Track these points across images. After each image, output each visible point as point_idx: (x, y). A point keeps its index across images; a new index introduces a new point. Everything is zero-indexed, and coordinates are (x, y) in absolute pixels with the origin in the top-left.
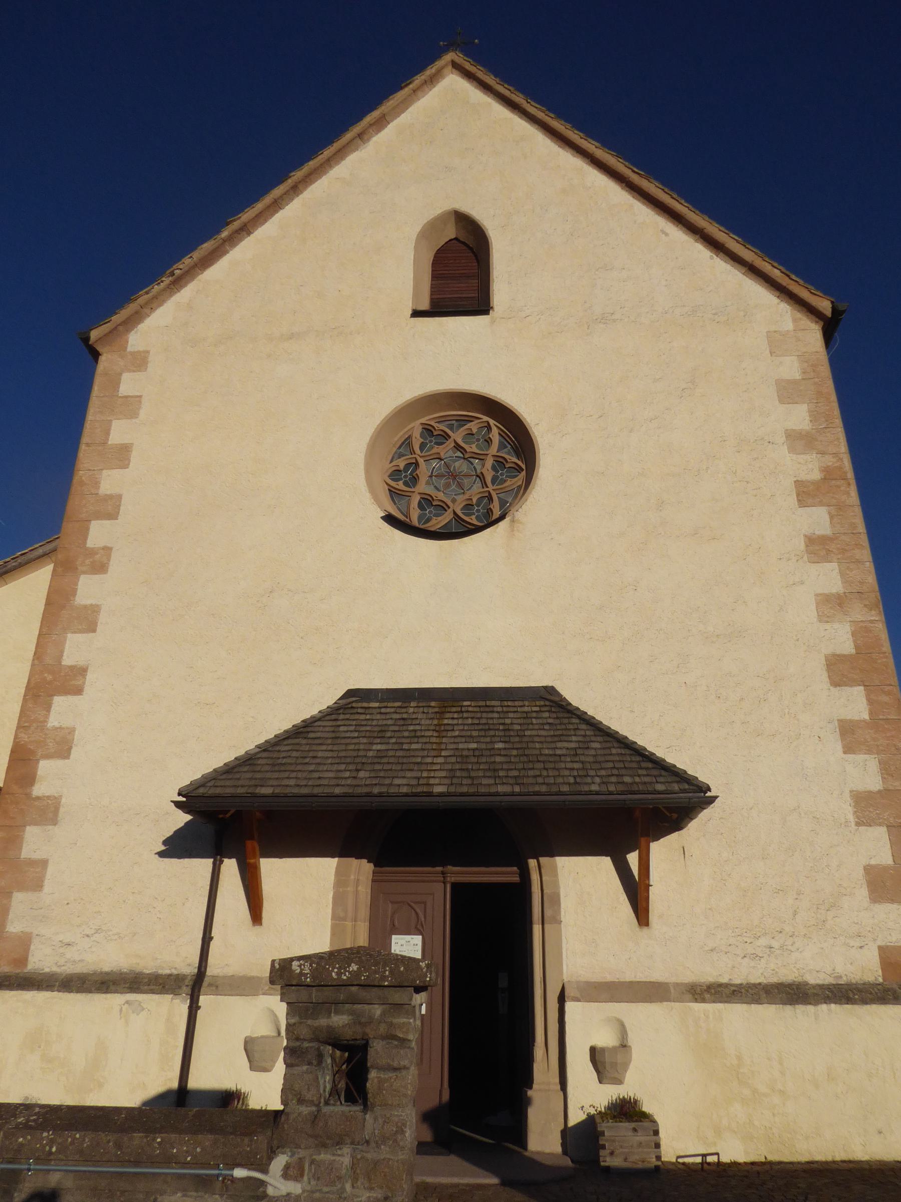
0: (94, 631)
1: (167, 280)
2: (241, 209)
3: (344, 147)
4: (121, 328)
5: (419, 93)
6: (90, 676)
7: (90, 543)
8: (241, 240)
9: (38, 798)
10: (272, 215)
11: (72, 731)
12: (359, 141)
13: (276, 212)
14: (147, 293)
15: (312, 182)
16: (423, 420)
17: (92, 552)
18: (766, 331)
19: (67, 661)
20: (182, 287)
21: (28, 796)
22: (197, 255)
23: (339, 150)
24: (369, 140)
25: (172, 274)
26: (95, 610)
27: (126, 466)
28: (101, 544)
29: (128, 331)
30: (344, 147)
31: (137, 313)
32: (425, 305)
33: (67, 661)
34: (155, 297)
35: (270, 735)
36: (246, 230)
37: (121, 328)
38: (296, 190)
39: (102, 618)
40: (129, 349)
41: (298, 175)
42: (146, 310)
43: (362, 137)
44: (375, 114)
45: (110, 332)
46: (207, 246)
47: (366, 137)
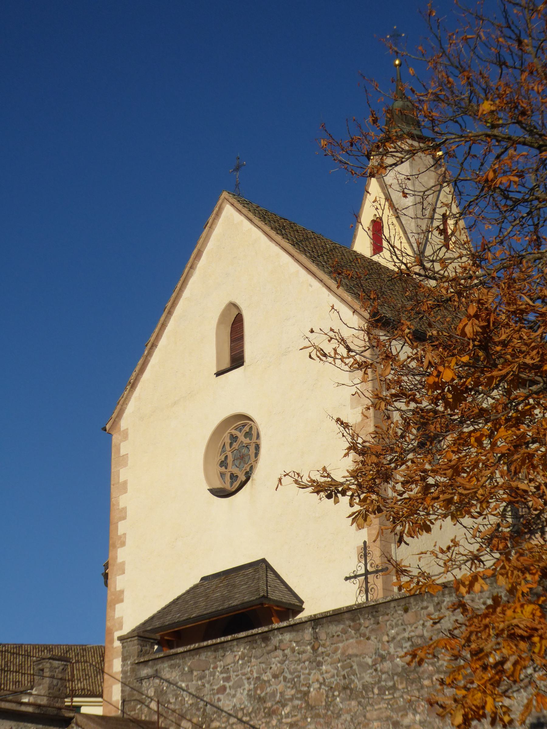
0: (124, 573)
1: (129, 387)
2: (150, 336)
3: (185, 278)
4: (117, 420)
5: (214, 226)
6: (125, 593)
7: (119, 534)
8: (154, 352)
9: (116, 648)
10: (164, 331)
11: (122, 618)
12: (192, 270)
13: (165, 329)
14: (123, 397)
15: (176, 304)
16: (228, 431)
17: (120, 537)
18: (370, 641)
19: (118, 589)
20: (136, 388)
21: (113, 647)
22: (137, 369)
23: (184, 282)
24: (196, 267)
25: (130, 383)
26: (123, 563)
27: (126, 492)
28: (122, 533)
29: (120, 419)
30: (185, 278)
31: (121, 409)
32: (226, 364)
33: (118, 589)
34: (126, 398)
35: (188, 588)
36: (154, 346)
37: (117, 420)
38: (170, 313)
39: (127, 567)
40: (122, 429)
41: (169, 304)
42: (124, 406)
43: (192, 267)
44: (195, 251)
45: (113, 423)
46: (140, 362)
47: (194, 266)
